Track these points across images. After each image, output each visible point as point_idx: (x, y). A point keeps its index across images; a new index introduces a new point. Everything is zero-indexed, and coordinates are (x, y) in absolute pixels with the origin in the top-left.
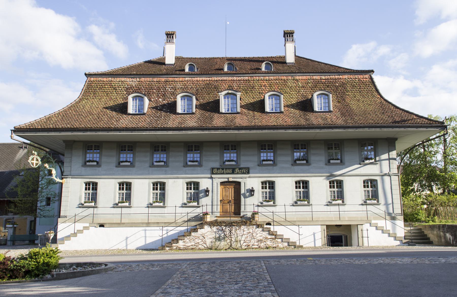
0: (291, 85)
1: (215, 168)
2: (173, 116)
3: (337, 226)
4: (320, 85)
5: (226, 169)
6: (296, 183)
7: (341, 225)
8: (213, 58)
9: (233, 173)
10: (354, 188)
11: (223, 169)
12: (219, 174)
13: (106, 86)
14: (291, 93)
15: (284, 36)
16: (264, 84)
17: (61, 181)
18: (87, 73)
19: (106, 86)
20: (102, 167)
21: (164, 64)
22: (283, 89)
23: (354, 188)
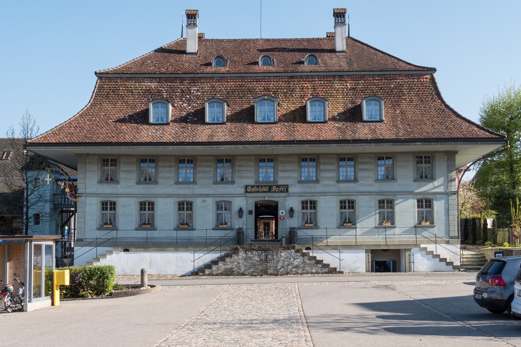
0: (337, 87)
1: (249, 186)
2: (200, 128)
3: (383, 250)
4: (372, 87)
5: (262, 186)
6: (341, 202)
7: (388, 250)
8: (245, 40)
9: (270, 191)
10: (406, 210)
11: (258, 187)
12: (254, 192)
13: (121, 88)
14: (338, 96)
15: (334, 16)
16: (306, 85)
17: (74, 200)
18: (98, 72)
19: (121, 88)
20: (121, 183)
21: (184, 52)
22: (329, 92)
23: (406, 210)
